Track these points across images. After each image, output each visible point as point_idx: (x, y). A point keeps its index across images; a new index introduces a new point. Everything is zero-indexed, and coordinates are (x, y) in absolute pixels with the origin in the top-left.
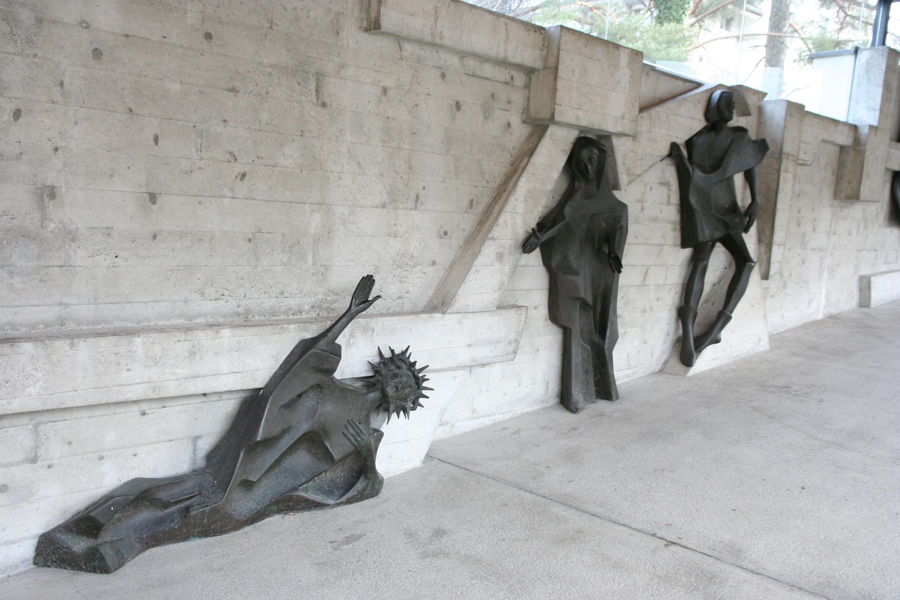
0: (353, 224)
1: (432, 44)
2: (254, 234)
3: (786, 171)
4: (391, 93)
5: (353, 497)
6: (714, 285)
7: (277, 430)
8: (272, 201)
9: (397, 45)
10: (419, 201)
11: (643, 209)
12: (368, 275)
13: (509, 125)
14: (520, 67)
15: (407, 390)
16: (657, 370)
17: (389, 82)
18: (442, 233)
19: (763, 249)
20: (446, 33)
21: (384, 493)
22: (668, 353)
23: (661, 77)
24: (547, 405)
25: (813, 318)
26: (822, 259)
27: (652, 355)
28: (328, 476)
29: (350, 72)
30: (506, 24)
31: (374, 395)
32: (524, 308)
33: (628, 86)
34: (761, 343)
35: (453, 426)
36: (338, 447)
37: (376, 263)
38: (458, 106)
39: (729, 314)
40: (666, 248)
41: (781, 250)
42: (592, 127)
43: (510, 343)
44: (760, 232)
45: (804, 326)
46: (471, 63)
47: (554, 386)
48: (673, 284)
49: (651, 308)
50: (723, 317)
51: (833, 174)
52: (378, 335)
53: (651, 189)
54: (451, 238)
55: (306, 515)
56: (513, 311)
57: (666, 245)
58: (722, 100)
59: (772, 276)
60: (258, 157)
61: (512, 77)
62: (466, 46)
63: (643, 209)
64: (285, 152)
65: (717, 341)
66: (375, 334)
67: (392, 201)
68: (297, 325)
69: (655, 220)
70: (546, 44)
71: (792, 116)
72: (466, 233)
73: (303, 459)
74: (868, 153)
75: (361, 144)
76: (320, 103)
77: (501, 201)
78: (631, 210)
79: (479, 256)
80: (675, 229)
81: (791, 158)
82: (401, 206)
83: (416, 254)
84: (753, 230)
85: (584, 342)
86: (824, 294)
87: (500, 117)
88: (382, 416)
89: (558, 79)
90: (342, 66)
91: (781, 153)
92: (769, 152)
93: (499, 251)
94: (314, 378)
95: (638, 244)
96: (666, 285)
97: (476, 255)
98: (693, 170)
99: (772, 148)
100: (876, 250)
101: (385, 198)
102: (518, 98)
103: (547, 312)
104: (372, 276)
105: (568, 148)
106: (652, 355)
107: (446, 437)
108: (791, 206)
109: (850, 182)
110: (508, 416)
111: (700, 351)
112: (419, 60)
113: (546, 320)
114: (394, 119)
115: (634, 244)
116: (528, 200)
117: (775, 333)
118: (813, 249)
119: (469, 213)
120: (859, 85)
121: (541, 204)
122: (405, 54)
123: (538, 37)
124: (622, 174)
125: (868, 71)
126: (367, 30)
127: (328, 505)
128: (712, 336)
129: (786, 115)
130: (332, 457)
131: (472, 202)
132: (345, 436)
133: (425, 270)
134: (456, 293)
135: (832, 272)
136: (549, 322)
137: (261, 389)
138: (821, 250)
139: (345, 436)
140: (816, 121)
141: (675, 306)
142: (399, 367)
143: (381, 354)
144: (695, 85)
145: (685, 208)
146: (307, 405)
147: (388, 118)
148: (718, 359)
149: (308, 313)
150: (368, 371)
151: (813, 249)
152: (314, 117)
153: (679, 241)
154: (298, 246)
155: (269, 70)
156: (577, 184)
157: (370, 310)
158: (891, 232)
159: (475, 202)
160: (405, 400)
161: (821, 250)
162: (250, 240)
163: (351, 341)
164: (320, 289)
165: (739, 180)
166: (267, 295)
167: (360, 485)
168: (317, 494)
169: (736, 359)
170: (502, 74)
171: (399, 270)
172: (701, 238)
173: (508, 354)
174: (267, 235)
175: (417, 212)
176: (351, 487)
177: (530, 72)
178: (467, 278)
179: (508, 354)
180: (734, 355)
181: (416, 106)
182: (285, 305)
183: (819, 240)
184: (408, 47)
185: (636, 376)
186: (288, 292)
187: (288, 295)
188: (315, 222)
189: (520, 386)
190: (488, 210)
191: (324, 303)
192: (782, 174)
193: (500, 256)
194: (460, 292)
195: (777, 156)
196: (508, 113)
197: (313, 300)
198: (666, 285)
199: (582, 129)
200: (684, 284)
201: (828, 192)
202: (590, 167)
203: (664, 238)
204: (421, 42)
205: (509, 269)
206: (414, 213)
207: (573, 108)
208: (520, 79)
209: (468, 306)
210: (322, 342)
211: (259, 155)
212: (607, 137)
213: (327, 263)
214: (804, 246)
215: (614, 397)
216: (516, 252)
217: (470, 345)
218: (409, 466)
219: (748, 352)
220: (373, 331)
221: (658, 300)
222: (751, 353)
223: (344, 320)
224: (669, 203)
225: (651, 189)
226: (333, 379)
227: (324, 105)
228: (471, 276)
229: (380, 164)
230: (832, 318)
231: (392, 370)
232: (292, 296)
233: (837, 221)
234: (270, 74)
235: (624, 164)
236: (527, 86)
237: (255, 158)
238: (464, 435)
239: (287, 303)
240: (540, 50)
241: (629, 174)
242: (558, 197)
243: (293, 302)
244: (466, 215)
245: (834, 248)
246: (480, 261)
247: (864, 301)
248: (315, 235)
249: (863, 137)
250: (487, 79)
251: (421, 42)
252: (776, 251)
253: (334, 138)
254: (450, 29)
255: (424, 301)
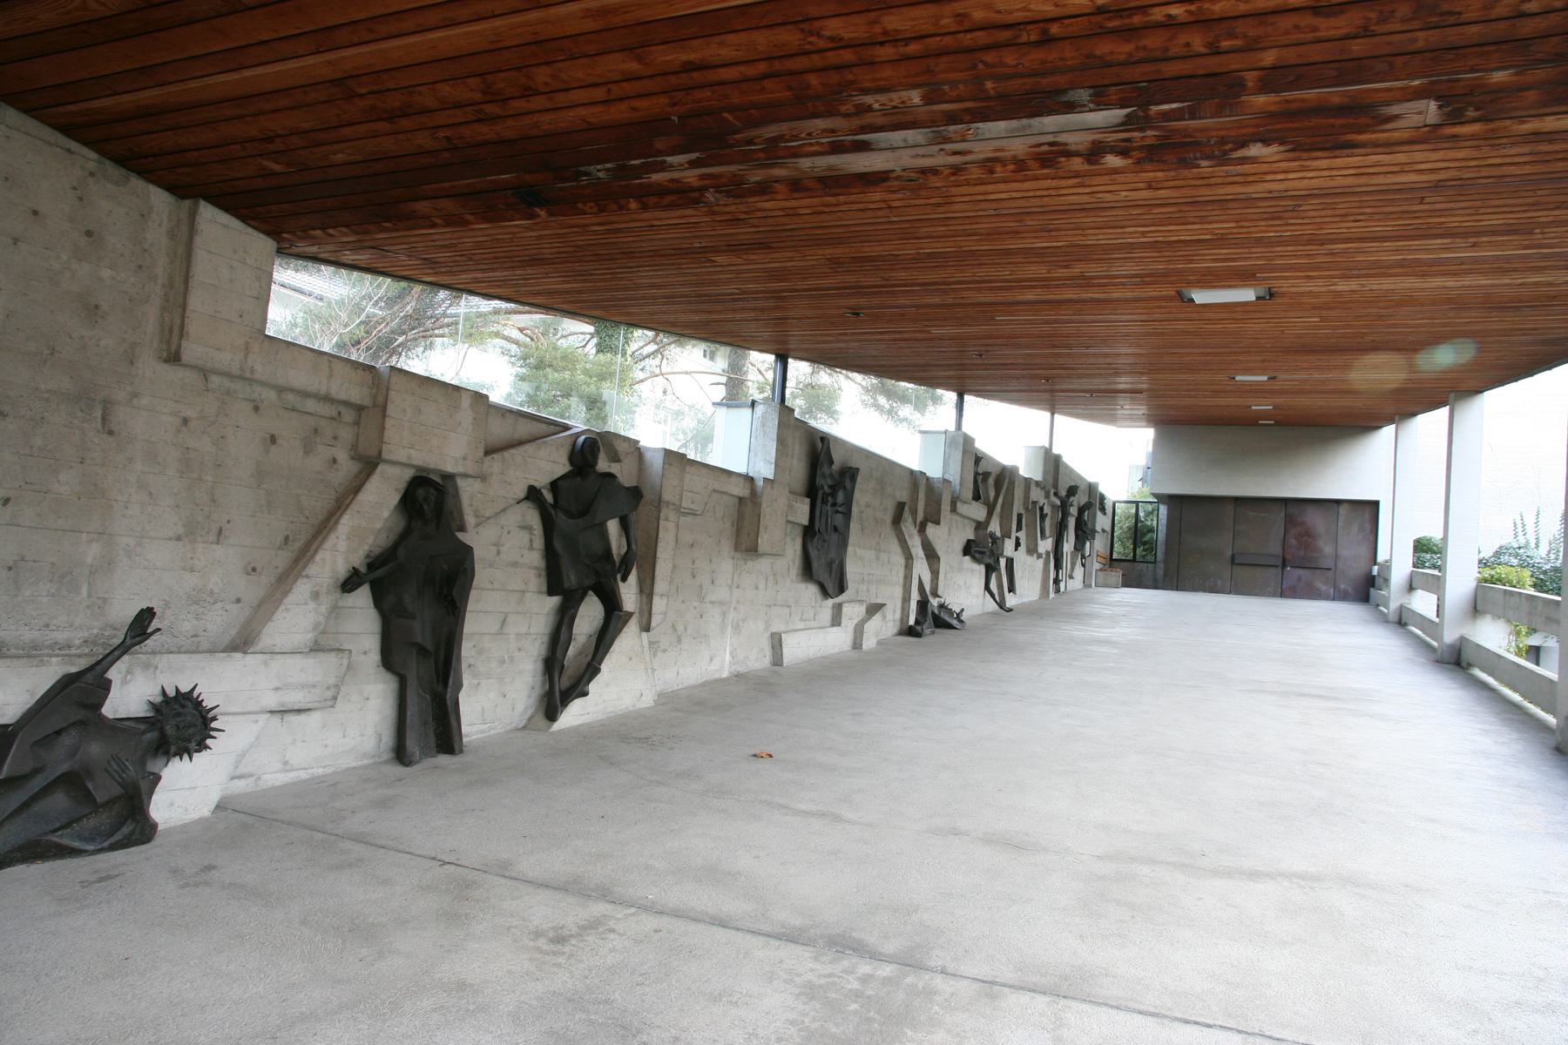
0: (140, 556)
1: (242, 378)
2: (15, 562)
3: (667, 519)
4: (192, 424)
5: (117, 842)
6: (590, 636)
7: (27, 769)
8: (41, 528)
9: (202, 377)
10: (222, 535)
11: (499, 553)
12: (148, 608)
13: (335, 461)
14: (346, 403)
15: (191, 731)
16: (521, 726)
17: (191, 413)
18: (250, 569)
19: (644, 599)
20: (259, 368)
21: (157, 840)
22: (534, 708)
23: (520, 419)
24: (380, 760)
25: (717, 676)
26: (724, 613)
27: (513, 710)
28: (90, 823)
29: (145, 401)
30: (330, 361)
31: (151, 736)
32: (347, 652)
33: (470, 428)
34: (643, 698)
35: (259, 778)
36: (103, 789)
37: (167, 598)
38: (273, 439)
39: (598, 666)
40: (528, 595)
41: (665, 601)
42: (427, 466)
43: (328, 688)
44: (641, 582)
45: (704, 684)
46: (290, 397)
47: (388, 739)
48: (539, 634)
49: (512, 659)
50: (592, 669)
51: (733, 526)
52: (162, 673)
53: (509, 533)
54: (260, 575)
55: (58, 864)
56: (333, 654)
57: (528, 591)
58: (586, 445)
59: (654, 629)
60: (27, 483)
61: (339, 413)
62: (281, 382)
63: (499, 553)
64: (60, 478)
65: (585, 694)
66: (158, 672)
67: (189, 533)
68: (60, 658)
69: (515, 564)
70: (376, 383)
71: (670, 465)
72: (279, 570)
73: (59, 801)
74: (764, 505)
75: (155, 473)
76: (106, 431)
77: (320, 539)
78: (477, 553)
79: (290, 595)
80: (540, 576)
81: (671, 507)
82: (199, 539)
83: (216, 590)
84: (633, 578)
85: (425, 692)
86: (728, 650)
87: (324, 452)
88: (161, 761)
89: (387, 418)
90: (135, 395)
91: (660, 500)
92: (643, 500)
93: (315, 589)
94: (81, 714)
95: (493, 590)
96: (529, 634)
97: (286, 593)
98: (556, 514)
99: (648, 495)
100: (789, 606)
101: (181, 530)
102: (346, 434)
103: (380, 658)
104: (152, 608)
105: (402, 486)
106: (513, 710)
107: (249, 790)
108: (674, 556)
109: (748, 534)
110: (330, 770)
111: (566, 705)
112: (228, 393)
113: (378, 666)
114: (195, 450)
115: (489, 589)
116: (352, 538)
117: (670, 690)
118: (712, 603)
119: (283, 549)
120: (756, 437)
121: (367, 543)
122: (211, 386)
123: (368, 376)
124: (469, 515)
125: (763, 425)
126: (167, 361)
127: (86, 851)
128: (579, 690)
129: (664, 463)
130: (95, 799)
131: (287, 538)
132: (108, 772)
133: (228, 607)
134: (260, 632)
135: (737, 628)
136: (382, 669)
137: (10, 725)
138: (721, 603)
139: (108, 772)
140: (704, 471)
141: (541, 658)
142: (183, 706)
143: (164, 692)
144: (561, 429)
145: (550, 554)
146: (67, 743)
147: (188, 448)
148: (588, 714)
149: (78, 648)
150: (147, 711)
151: (712, 603)
152: (98, 445)
153: (545, 588)
154: (69, 577)
155: (46, 395)
156: (413, 524)
157: (150, 643)
158: (807, 588)
159: (291, 539)
160: (189, 741)
161: (721, 603)
162: (10, 568)
163: (128, 678)
164: (96, 624)
165: (613, 527)
166: (27, 628)
167: (125, 830)
168: (73, 841)
169: (611, 714)
170: (326, 410)
171: (196, 606)
172: (566, 585)
173: (325, 700)
174: (32, 564)
175: (219, 547)
176: (112, 835)
177: (359, 409)
178: (274, 616)
179: (325, 700)
180: (608, 710)
181: (222, 437)
182: (51, 639)
183: (721, 593)
184: (215, 380)
185: (492, 732)
186: (55, 625)
187: (54, 628)
188: (93, 552)
189: (344, 737)
190: (305, 547)
191: (100, 639)
192: (662, 523)
193: (315, 596)
194: (264, 631)
195: (656, 504)
196: (334, 449)
197: (86, 634)
198: (529, 634)
199: (419, 468)
200: (550, 634)
201: (727, 545)
202: (426, 507)
203: (526, 584)
204: (228, 375)
205: (326, 608)
206: (215, 547)
207: (404, 447)
208: (348, 416)
209: (274, 645)
210: (88, 675)
211: (27, 480)
212: (449, 478)
213: (107, 596)
214: (701, 599)
215: (457, 752)
216: (335, 592)
217: (277, 689)
218: (194, 815)
219: (628, 708)
220: (156, 668)
221: (520, 650)
222: (631, 708)
223: (117, 653)
224: (531, 548)
225: (509, 533)
226: (101, 715)
227: (111, 433)
228: (279, 615)
229: (175, 494)
230: (738, 676)
231: (175, 709)
232: (61, 629)
233: (740, 574)
234: (47, 400)
235: (471, 505)
236: (357, 423)
237: (23, 484)
238: (274, 788)
239: (53, 637)
240: (369, 387)
241: (477, 516)
242: (393, 537)
243: (61, 636)
244: (280, 552)
245: (738, 602)
246: (291, 598)
247: (777, 660)
248: (92, 566)
249: (759, 490)
250: (310, 414)
251: (228, 375)
252: (657, 601)
253: (121, 466)
254: (263, 364)
255: (226, 639)
